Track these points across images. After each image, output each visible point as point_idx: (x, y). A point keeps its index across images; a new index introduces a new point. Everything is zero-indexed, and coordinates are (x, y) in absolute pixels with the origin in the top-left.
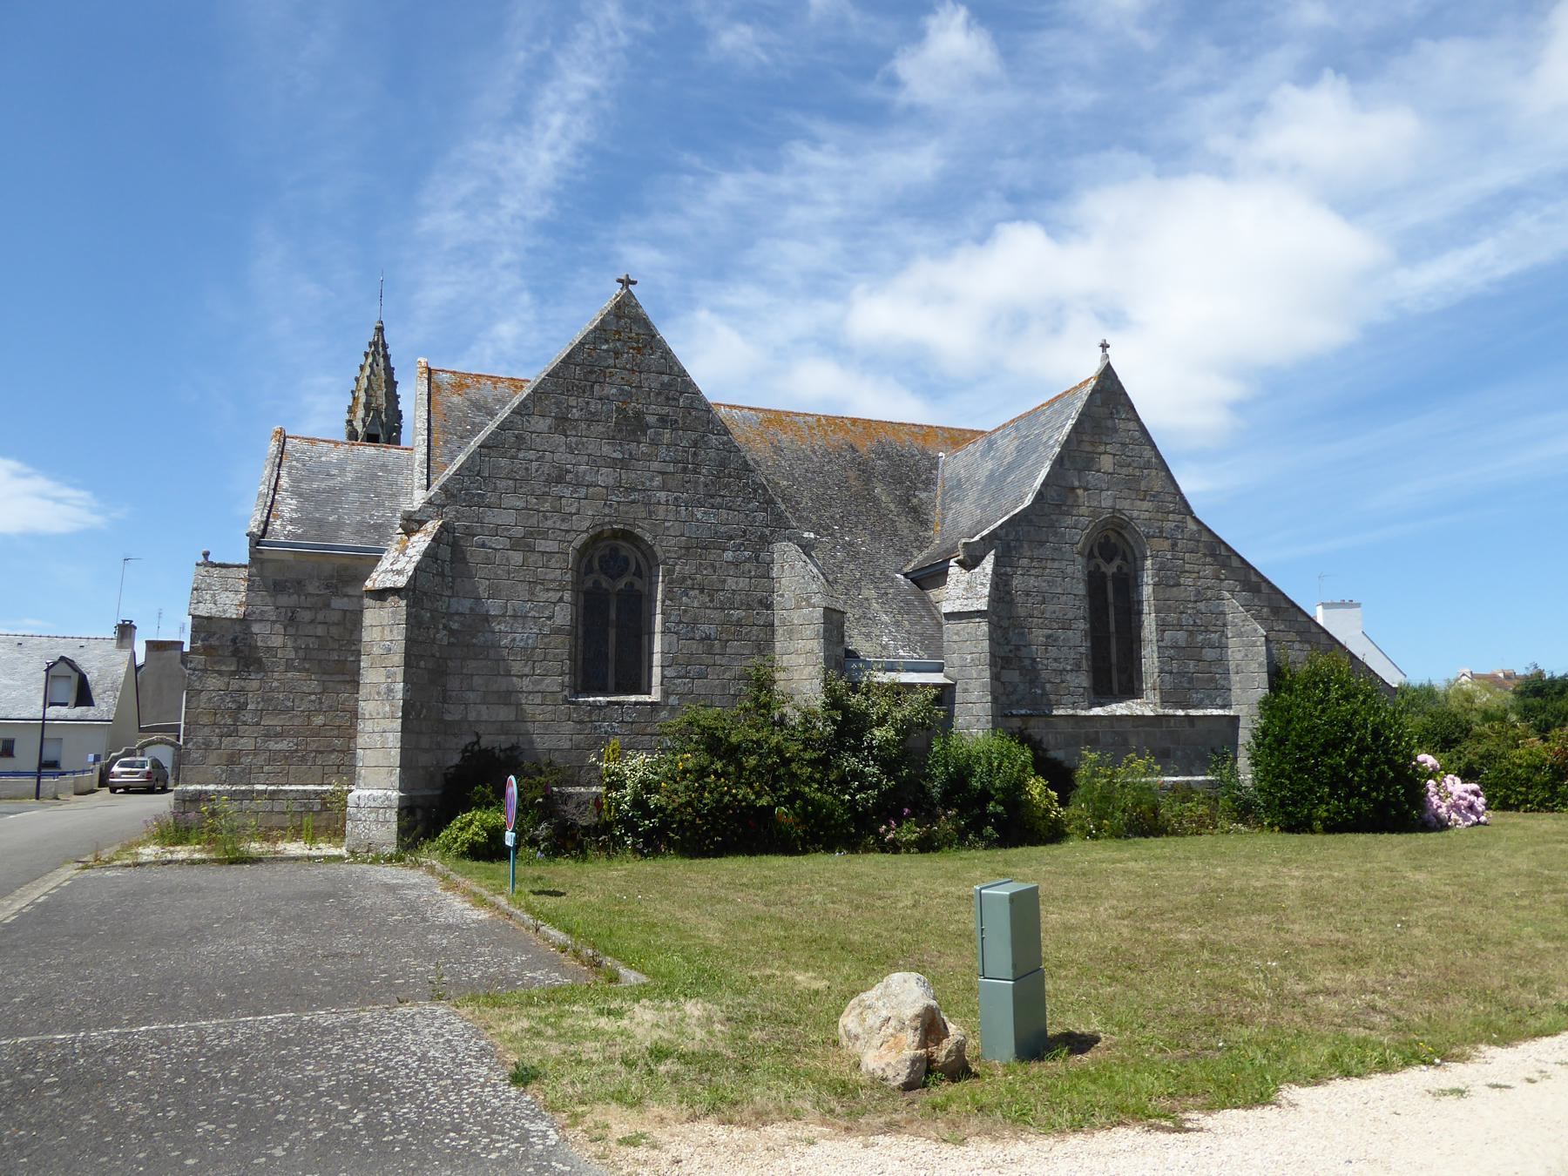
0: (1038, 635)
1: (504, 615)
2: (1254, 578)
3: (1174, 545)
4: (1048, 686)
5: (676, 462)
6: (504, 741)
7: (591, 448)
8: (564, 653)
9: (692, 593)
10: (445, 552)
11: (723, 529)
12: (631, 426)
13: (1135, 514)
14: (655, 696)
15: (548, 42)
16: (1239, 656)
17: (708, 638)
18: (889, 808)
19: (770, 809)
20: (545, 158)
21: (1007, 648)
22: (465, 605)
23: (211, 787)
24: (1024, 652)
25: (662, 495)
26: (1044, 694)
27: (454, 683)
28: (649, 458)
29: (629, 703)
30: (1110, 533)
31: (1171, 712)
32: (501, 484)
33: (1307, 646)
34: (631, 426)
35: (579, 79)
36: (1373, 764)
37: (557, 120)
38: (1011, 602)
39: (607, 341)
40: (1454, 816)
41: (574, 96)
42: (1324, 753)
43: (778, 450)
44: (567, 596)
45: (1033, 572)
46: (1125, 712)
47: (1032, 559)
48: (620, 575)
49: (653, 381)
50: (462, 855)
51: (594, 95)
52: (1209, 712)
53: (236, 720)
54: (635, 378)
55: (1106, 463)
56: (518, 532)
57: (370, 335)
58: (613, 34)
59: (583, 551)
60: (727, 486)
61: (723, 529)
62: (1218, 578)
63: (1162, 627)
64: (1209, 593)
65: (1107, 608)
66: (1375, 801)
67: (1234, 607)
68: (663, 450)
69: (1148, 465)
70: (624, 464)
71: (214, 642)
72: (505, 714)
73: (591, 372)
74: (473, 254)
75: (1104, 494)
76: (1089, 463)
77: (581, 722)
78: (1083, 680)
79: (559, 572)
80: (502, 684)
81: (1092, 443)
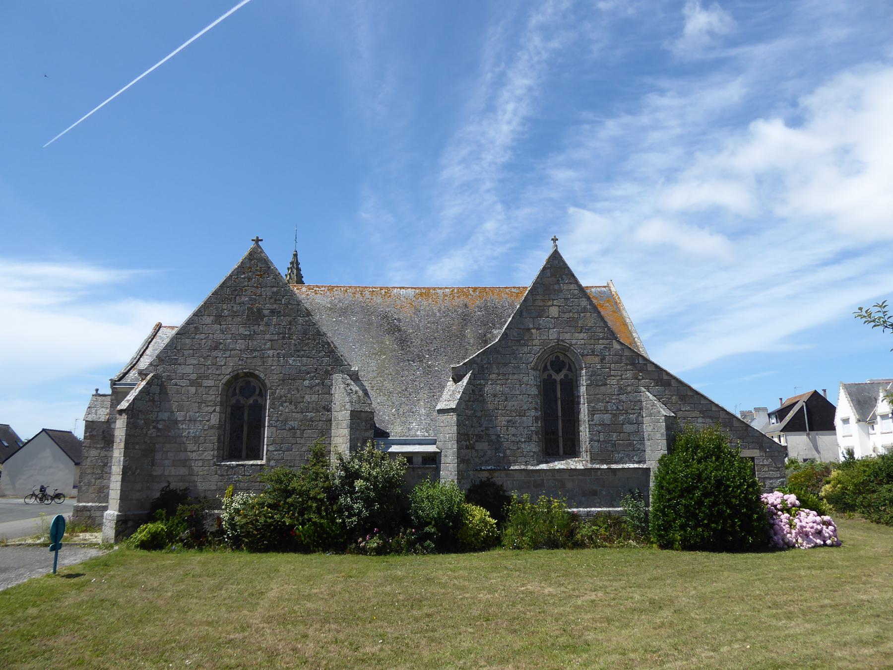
0: (502, 420)
1: (185, 420)
2: (665, 377)
3: (603, 360)
4: (508, 451)
5: (279, 334)
6: (181, 486)
7: (233, 330)
8: (215, 439)
9: (285, 404)
10: (156, 389)
11: (304, 368)
12: (255, 316)
13: (574, 342)
14: (264, 462)
15: (503, 65)
16: (650, 429)
17: (293, 428)
18: (365, 528)
19: (292, 526)
20: (505, 128)
21: (480, 429)
22: (165, 416)
23: (90, 504)
24: (491, 431)
25: (271, 352)
26: (505, 456)
27: (158, 456)
28: (264, 333)
29: (248, 465)
30: (559, 354)
31: (597, 466)
32: (186, 353)
33: (709, 420)
34: (255, 316)
35: (521, 81)
36: (715, 504)
37: (510, 107)
38: (484, 401)
39: (244, 273)
40: (800, 540)
41: (519, 92)
42: (681, 496)
43: (417, 311)
44: (218, 409)
45: (499, 382)
46: (562, 467)
47: (499, 374)
48: (251, 396)
49: (268, 292)
50: (137, 547)
51: (530, 89)
52: (626, 466)
53: (102, 471)
54: (258, 291)
55: (554, 311)
56: (194, 377)
57: (291, 259)
58: (538, 53)
59: (228, 384)
60: (307, 344)
61: (304, 368)
62: (637, 378)
63: (592, 412)
64: (629, 389)
65: (556, 401)
66: (715, 530)
67: (648, 397)
68: (272, 328)
69: (584, 310)
70: (250, 337)
71: (94, 433)
72: (183, 471)
73: (235, 290)
74: (470, 187)
75: (551, 331)
76: (542, 312)
77: (222, 475)
78: (533, 447)
79: (213, 396)
80: (182, 456)
81: (543, 301)
